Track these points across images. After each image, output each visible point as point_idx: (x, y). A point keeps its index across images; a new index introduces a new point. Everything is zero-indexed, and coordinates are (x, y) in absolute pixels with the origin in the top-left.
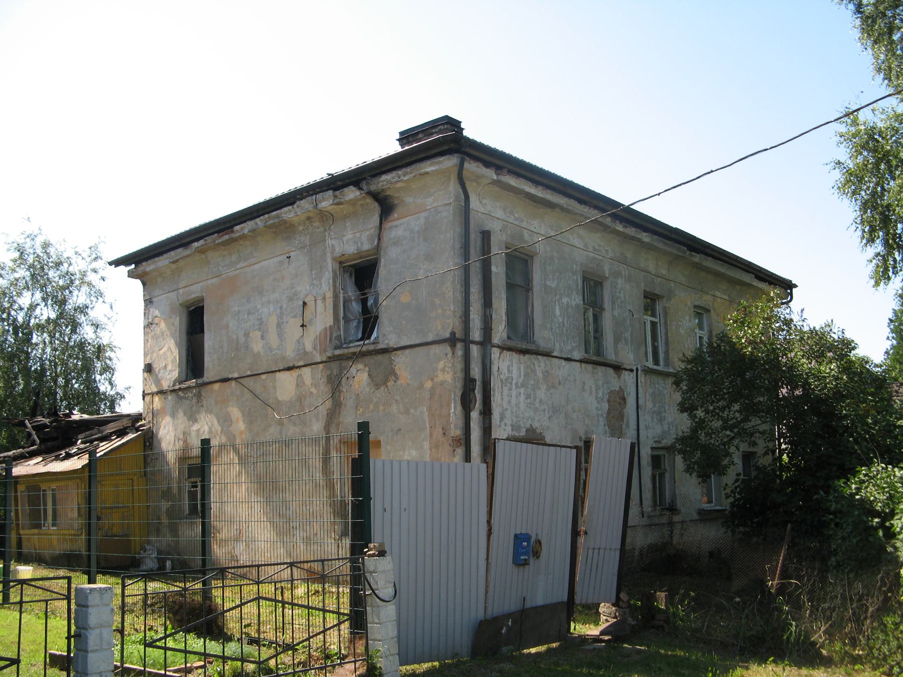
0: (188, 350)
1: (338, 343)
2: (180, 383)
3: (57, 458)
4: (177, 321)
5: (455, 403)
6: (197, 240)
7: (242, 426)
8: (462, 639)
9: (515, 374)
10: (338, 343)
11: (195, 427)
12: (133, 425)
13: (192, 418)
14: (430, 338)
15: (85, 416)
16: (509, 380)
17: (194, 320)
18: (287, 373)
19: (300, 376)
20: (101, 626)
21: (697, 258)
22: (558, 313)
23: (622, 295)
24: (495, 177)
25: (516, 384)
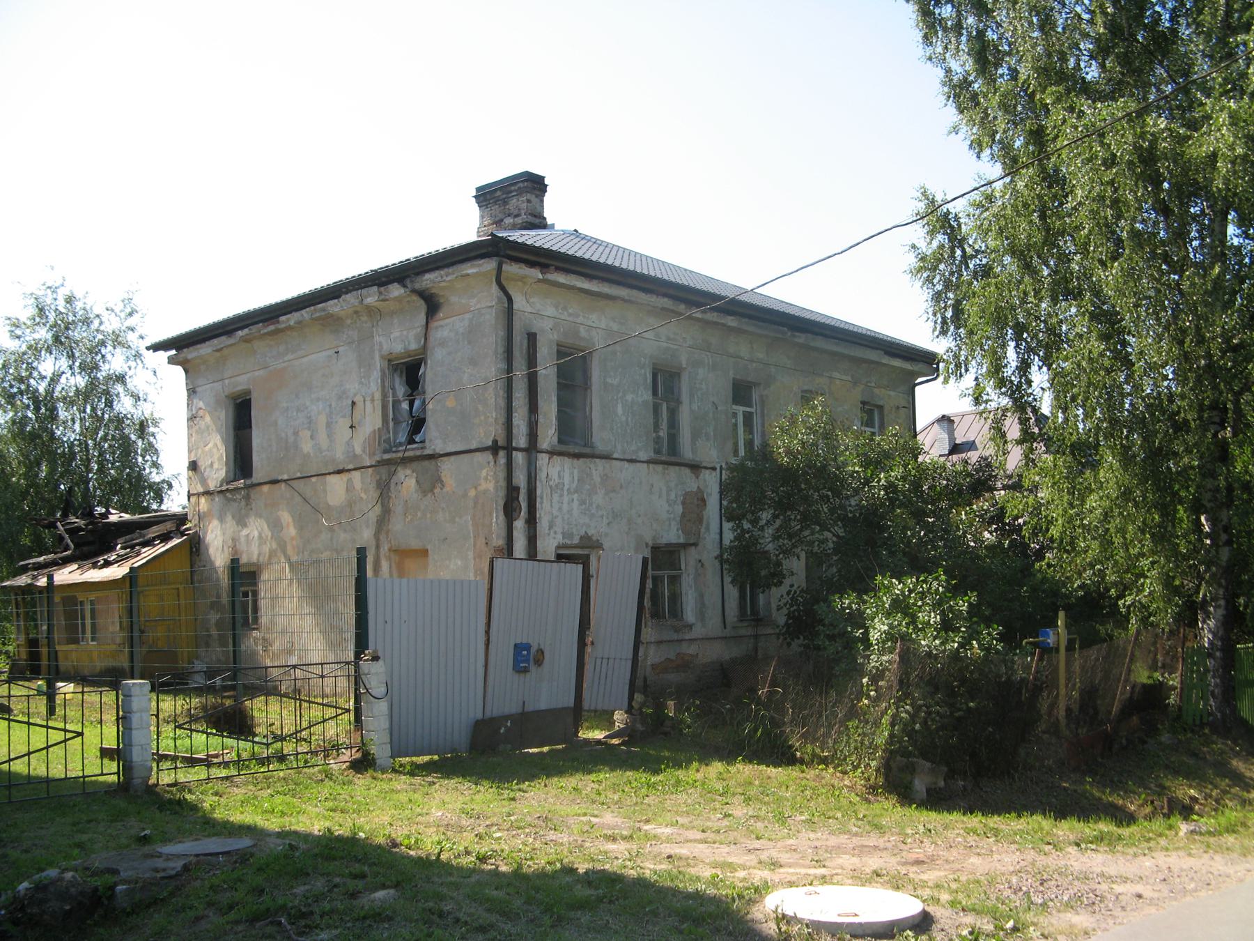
0: (235, 447)
2: (228, 483)
3: (95, 566)
4: (223, 415)
7: (292, 531)
8: (460, 735)
9: (567, 480)
11: (245, 532)
12: (178, 529)
13: (241, 522)
14: (474, 446)
15: (126, 516)
16: (559, 487)
17: (241, 415)
18: (337, 476)
19: (349, 480)
20: (141, 711)
21: (801, 338)
22: (620, 410)
23: (704, 386)
24: (540, 276)
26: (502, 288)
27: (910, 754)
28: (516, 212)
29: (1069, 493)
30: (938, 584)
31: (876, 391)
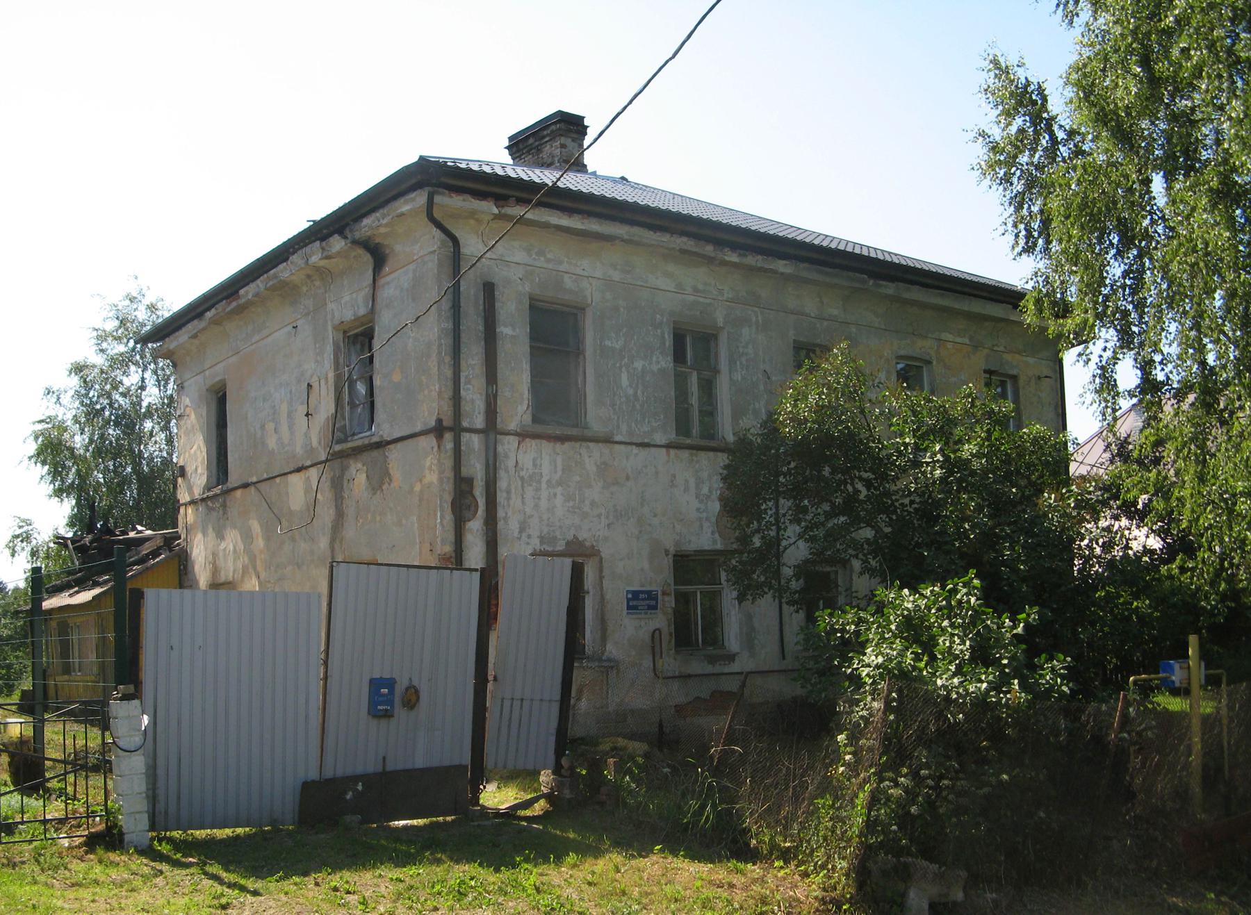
1: (342, 436)
2: (209, 490)
5: (442, 511)
6: (209, 309)
8: (285, 803)
10: (342, 436)
11: (223, 546)
14: (418, 428)
23: (750, 350)
24: (496, 211)
25: (549, 481)
26: (439, 225)
27: (899, 852)
28: (550, 161)
29: (1197, 462)
30: (968, 591)
31: (1008, 357)
